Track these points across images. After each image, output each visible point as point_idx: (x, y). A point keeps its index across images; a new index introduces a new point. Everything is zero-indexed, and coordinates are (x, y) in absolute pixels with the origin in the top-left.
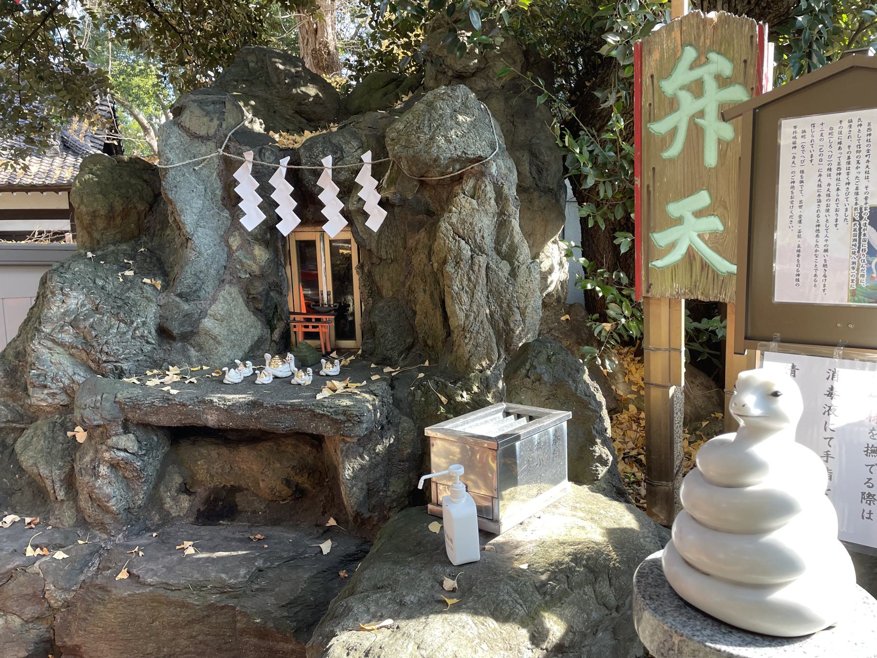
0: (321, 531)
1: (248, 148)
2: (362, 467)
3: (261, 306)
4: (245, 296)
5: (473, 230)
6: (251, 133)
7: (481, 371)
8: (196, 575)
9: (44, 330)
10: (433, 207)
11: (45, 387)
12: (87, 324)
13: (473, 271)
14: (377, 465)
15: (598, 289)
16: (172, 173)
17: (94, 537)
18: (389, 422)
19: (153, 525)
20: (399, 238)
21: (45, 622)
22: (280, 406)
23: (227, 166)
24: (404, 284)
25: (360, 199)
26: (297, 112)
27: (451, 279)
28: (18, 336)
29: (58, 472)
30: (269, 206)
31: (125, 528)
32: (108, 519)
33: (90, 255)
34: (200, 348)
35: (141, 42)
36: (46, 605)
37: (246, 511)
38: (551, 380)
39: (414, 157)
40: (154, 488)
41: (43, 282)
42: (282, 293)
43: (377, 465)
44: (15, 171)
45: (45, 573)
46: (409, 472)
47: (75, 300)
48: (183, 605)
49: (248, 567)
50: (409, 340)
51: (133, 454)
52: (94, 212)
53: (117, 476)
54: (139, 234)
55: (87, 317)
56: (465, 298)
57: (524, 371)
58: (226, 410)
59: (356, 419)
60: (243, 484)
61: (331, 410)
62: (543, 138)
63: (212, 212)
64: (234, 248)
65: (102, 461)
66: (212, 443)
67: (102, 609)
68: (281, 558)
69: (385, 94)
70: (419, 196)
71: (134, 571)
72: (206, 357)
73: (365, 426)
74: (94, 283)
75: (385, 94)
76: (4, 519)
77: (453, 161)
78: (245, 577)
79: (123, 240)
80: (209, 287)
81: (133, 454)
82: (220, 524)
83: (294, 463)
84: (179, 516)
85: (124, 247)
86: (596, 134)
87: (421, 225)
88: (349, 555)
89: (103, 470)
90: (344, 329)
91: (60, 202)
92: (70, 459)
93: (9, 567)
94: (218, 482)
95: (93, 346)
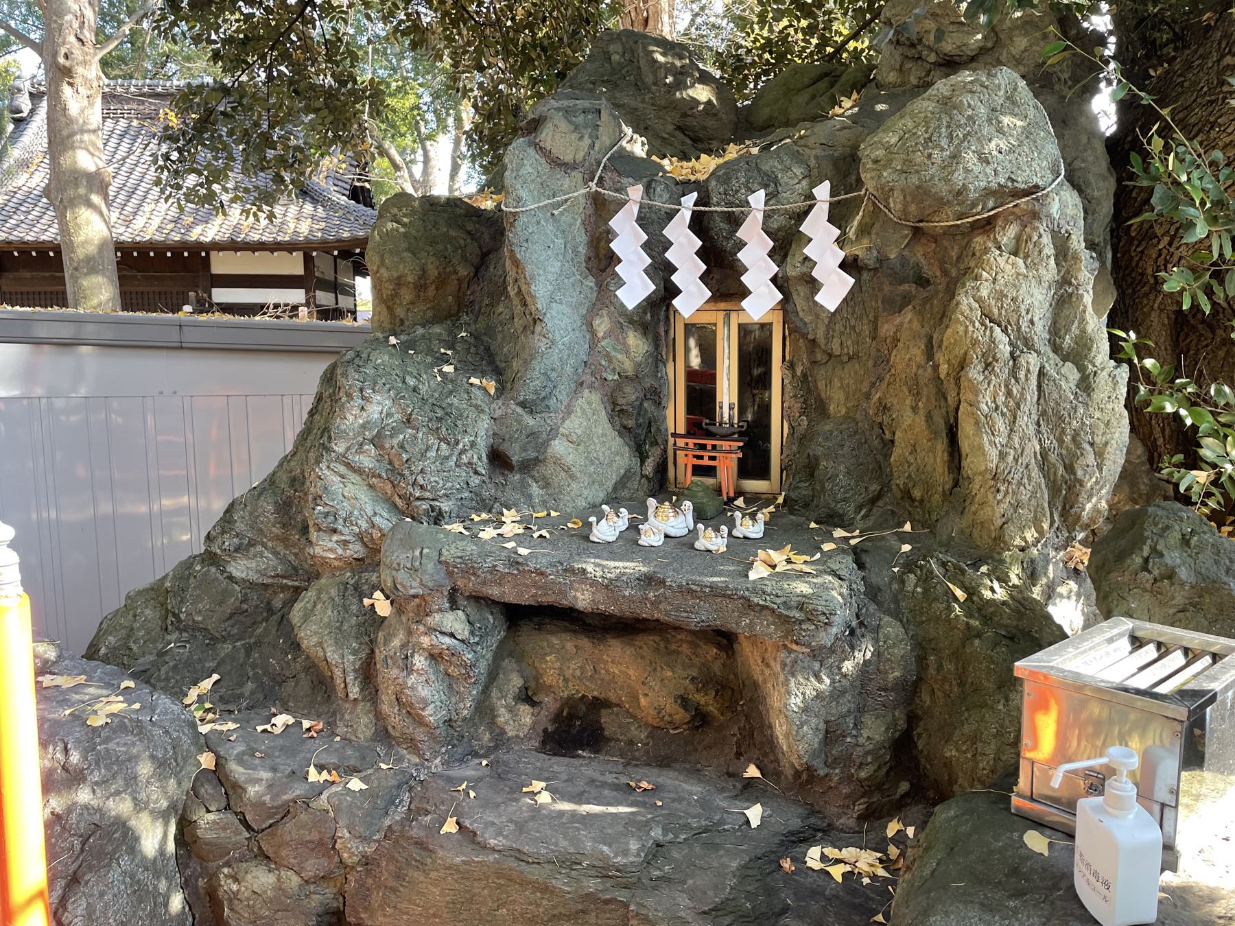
0: (739, 786)
1: (631, 180)
2: (819, 695)
3: (631, 423)
4: (609, 409)
5: (1017, 311)
6: (630, 158)
7: (1022, 550)
8: (564, 843)
9: (336, 448)
10: (931, 271)
11: (335, 531)
12: (395, 442)
13: (1017, 380)
14: (843, 693)
15: (1183, 412)
16: (523, 219)
17: (400, 760)
18: (861, 624)
19: (482, 748)
20: (865, 321)
21: (332, 884)
22: (694, 587)
23: (596, 210)
24: (868, 396)
25: (807, 259)
26: (679, 128)
27: (976, 393)
28: (294, 454)
29: (351, 658)
30: (662, 270)
31: (443, 750)
32: (420, 735)
33: (393, 340)
34: (546, 484)
35: (426, 40)
36: (336, 859)
37: (618, 740)
38: (1193, 580)
39: (918, 187)
40: (483, 692)
41: (329, 378)
42: (660, 403)
43: (843, 693)
44: (258, 220)
45: (337, 810)
46: (894, 709)
47: (379, 407)
48: (546, 889)
49: (640, 838)
50: (874, 487)
51: (463, 641)
52: (399, 278)
53: (437, 672)
54: (458, 311)
55: (395, 432)
56: (1001, 424)
57: (1138, 560)
58: (607, 586)
59: (823, 618)
60: (613, 698)
61: (778, 601)
62: (1091, 159)
63: (572, 280)
64: (600, 335)
65: (418, 647)
66: (566, 630)
67: (422, 878)
68: (686, 827)
69: (813, 97)
70: (906, 253)
71: (467, 823)
72: (553, 495)
73: (834, 630)
74: (404, 382)
75: (813, 97)
76: (273, 721)
77: (988, 192)
78: (638, 855)
79: (436, 320)
80: (562, 394)
81: (463, 641)
82: (579, 756)
83: (694, 672)
84: (517, 736)
85: (437, 329)
86: (1202, 151)
87: (906, 300)
88: (791, 833)
89: (419, 661)
90: (754, 462)
91: (293, 265)
92: (367, 639)
93: (285, 797)
94: (574, 689)
95: (402, 475)
